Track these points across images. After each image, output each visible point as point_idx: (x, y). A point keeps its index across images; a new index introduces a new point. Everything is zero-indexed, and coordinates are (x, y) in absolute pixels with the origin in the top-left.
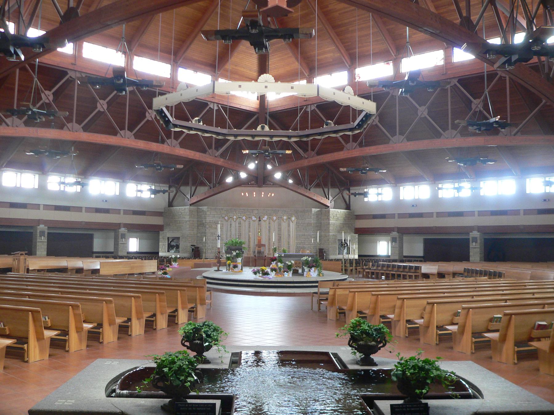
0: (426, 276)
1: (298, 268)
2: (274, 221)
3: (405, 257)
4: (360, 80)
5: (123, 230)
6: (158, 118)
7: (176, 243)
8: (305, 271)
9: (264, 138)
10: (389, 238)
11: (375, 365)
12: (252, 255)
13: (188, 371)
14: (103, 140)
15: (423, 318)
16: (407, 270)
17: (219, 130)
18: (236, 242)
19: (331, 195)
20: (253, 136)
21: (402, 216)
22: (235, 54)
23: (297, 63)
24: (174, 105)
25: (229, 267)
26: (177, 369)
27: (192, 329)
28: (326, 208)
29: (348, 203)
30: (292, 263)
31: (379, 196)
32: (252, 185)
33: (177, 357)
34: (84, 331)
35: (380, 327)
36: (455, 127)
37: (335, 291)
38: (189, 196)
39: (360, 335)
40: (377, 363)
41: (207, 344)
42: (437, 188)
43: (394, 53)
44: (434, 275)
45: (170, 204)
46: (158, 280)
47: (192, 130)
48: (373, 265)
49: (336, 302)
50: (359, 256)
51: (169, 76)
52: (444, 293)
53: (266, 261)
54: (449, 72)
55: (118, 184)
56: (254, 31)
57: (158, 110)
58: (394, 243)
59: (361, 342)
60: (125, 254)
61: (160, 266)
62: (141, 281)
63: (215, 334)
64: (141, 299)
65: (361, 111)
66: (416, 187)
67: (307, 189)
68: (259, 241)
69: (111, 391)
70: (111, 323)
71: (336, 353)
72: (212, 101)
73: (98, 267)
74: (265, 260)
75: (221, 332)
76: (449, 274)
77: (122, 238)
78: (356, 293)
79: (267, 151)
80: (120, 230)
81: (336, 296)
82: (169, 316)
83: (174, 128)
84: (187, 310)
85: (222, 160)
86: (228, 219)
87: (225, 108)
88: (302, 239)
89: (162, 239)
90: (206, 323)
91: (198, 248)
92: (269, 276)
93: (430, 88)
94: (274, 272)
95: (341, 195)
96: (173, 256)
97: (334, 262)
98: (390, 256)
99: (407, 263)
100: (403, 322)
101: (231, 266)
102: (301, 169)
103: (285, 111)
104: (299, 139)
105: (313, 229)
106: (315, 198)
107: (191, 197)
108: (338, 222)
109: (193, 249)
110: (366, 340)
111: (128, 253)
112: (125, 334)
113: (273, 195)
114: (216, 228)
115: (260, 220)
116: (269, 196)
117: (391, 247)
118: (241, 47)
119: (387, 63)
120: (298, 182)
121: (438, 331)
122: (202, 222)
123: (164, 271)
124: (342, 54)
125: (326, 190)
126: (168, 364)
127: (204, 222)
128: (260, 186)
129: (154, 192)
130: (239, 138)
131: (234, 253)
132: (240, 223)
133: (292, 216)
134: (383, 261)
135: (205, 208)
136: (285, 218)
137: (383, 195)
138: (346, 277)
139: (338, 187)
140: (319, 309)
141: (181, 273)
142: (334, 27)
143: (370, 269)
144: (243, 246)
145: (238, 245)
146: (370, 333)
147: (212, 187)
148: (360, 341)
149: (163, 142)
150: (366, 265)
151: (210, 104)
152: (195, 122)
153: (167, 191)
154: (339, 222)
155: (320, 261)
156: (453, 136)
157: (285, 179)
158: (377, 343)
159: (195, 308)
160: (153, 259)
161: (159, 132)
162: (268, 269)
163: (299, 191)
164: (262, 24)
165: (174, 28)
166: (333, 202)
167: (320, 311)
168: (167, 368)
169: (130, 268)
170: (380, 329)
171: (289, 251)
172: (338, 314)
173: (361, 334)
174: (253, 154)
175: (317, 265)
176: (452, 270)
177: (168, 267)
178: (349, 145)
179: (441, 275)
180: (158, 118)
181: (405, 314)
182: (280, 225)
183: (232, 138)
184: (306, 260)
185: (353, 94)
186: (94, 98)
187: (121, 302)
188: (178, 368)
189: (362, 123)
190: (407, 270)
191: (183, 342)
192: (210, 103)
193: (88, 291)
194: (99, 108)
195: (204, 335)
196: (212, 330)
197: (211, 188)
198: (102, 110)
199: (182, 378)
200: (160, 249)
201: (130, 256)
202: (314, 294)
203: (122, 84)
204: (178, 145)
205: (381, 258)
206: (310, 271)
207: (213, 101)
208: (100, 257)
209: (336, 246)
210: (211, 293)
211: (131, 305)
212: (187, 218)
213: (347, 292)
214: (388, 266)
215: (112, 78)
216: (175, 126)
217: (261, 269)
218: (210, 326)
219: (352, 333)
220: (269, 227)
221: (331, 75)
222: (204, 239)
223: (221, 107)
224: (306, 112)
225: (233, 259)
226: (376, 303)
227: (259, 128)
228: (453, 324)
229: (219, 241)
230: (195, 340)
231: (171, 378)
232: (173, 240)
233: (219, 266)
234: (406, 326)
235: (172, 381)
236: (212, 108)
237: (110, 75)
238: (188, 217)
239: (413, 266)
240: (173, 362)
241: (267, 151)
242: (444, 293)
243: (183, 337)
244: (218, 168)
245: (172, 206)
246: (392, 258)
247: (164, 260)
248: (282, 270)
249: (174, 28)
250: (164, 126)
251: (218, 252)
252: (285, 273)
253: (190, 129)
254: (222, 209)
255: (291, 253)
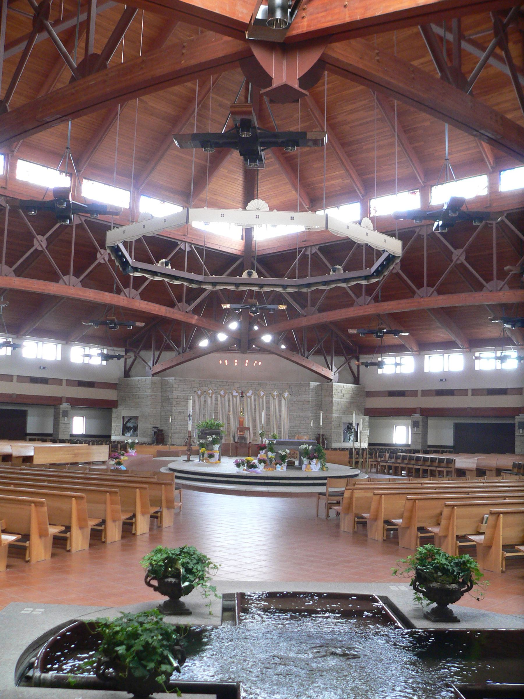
0: (461, 473)
1: (293, 460)
2: (261, 397)
3: (430, 446)
4: (377, 214)
5: (65, 406)
6: (113, 258)
7: (133, 424)
8: (303, 463)
9: (252, 288)
10: (409, 422)
11: (456, 620)
12: (232, 442)
13: (162, 653)
14: (40, 287)
15: (439, 524)
16: (436, 464)
17: (192, 276)
18: (212, 424)
19: (335, 366)
20: (237, 285)
21: (426, 393)
22: (214, 179)
23: (294, 192)
24: (134, 240)
25: (203, 457)
26: (141, 648)
27: (164, 560)
28: (328, 382)
29: (356, 376)
30: (286, 453)
31: (398, 366)
32: (233, 351)
33: (141, 624)
34: (2, 545)
35: (463, 559)
36: (502, 275)
37: (353, 492)
38: (150, 364)
39: (432, 573)
40: (459, 618)
41: (187, 584)
42: (474, 357)
43: (422, 180)
44: (491, 470)
45: (127, 374)
46: (109, 473)
47: (157, 276)
48: (390, 457)
49: (354, 507)
50: (370, 444)
51: (128, 207)
52: (505, 498)
53: (251, 449)
54: (494, 205)
55: (60, 346)
56: (245, 135)
57: (113, 247)
58: (415, 428)
59: (435, 585)
60: (68, 437)
61: (113, 454)
62: (86, 474)
63: (199, 568)
64: (85, 500)
65: (379, 253)
66: (446, 355)
67: (304, 356)
68: (242, 423)
69: (27, 664)
70: (43, 534)
71: (386, 597)
72: (184, 240)
73: (31, 453)
74: (249, 448)
75: (209, 563)
76: (491, 470)
77: (64, 416)
78: (383, 496)
79: (254, 305)
80: (61, 406)
81: (354, 499)
82: (124, 524)
83: (133, 273)
84: (149, 516)
85: (196, 317)
86: (202, 394)
87: (200, 250)
88: (296, 422)
89: (116, 419)
90: (185, 550)
91: (162, 430)
92: (256, 469)
93: (476, 220)
94: (262, 464)
95: (348, 365)
96: (130, 441)
97: (338, 452)
98: (410, 445)
99: (434, 454)
100: (453, 538)
101: (206, 456)
102: (298, 331)
103: (278, 255)
104: (297, 290)
105: (311, 409)
106: (314, 368)
107: (153, 365)
108: (342, 400)
109: (155, 433)
110: (442, 581)
111: (72, 436)
112: (61, 548)
113: (260, 363)
114: (186, 406)
115: (242, 396)
116: (254, 364)
117: (412, 433)
118: (222, 169)
119: (413, 193)
120: (293, 347)
121: (505, 553)
122: (167, 397)
123: (118, 460)
124: (353, 180)
125: (329, 358)
126: (124, 639)
127: (170, 397)
128: (243, 352)
129: (107, 357)
130: (219, 287)
131: (210, 439)
132: (217, 400)
133: (284, 392)
134: (402, 451)
135: (171, 379)
136: (275, 393)
137: (402, 366)
138: (357, 472)
139: (344, 355)
140: (328, 516)
141: (141, 463)
142: (343, 145)
143: (387, 462)
144: (221, 428)
145: (214, 428)
146: (449, 570)
147: (181, 352)
148: (432, 582)
149: (119, 292)
150: (380, 456)
151: (181, 244)
152: (161, 265)
153: (122, 357)
154: (345, 400)
155: (323, 451)
156: (499, 288)
157: (276, 342)
158: (459, 586)
159: (159, 513)
160: (104, 444)
161: (112, 278)
162: (255, 461)
163: (293, 359)
164: (257, 126)
165: (135, 144)
166: (337, 375)
167: (329, 518)
168: (124, 647)
169: (73, 456)
170: (464, 563)
171: (280, 437)
172: (356, 524)
173: (433, 571)
174: (235, 309)
175: (320, 455)
176: (495, 465)
177: (123, 455)
178: (361, 300)
179: (481, 472)
180: (113, 258)
181: (455, 528)
182: (268, 402)
183: (209, 288)
184: (306, 449)
185: (372, 228)
186: (30, 233)
187: (57, 503)
188: (143, 646)
189: (382, 269)
190: (428, 463)
191: (149, 579)
192: (181, 242)
193: (12, 488)
194: (36, 246)
195: (182, 570)
196: (195, 561)
197: (179, 354)
198: (40, 248)
199: (151, 665)
200: (113, 432)
201: (74, 439)
202: (321, 496)
203: (66, 209)
204: (139, 296)
205: (399, 448)
206: (310, 463)
207: (185, 240)
208: (452, 453)
209: (340, 431)
210: (180, 493)
211: (71, 508)
212: (149, 392)
213: (369, 494)
214: (411, 458)
215: (52, 201)
216: (136, 269)
217: (246, 460)
218: (192, 555)
219: (420, 569)
220: (255, 405)
221: (338, 208)
222: (170, 419)
223: (195, 247)
224: (305, 256)
225: (207, 446)
226: (412, 511)
227: (245, 275)
228: (479, 533)
229: (191, 421)
230: (168, 577)
231: (131, 665)
232: (129, 421)
233: (190, 455)
234: (456, 544)
235: (132, 671)
236: (184, 249)
237: (50, 198)
238: (150, 390)
239: (436, 458)
240: (135, 635)
241: (254, 305)
242: (505, 498)
243: (149, 571)
244: (189, 327)
245: (129, 377)
246: (413, 448)
247: (117, 445)
248: (274, 462)
249: (135, 144)
250: (121, 269)
251: (189, 437)
252: (278, 465)
253: (155, 274)
254: (194, 381)
255: (282, 440)
